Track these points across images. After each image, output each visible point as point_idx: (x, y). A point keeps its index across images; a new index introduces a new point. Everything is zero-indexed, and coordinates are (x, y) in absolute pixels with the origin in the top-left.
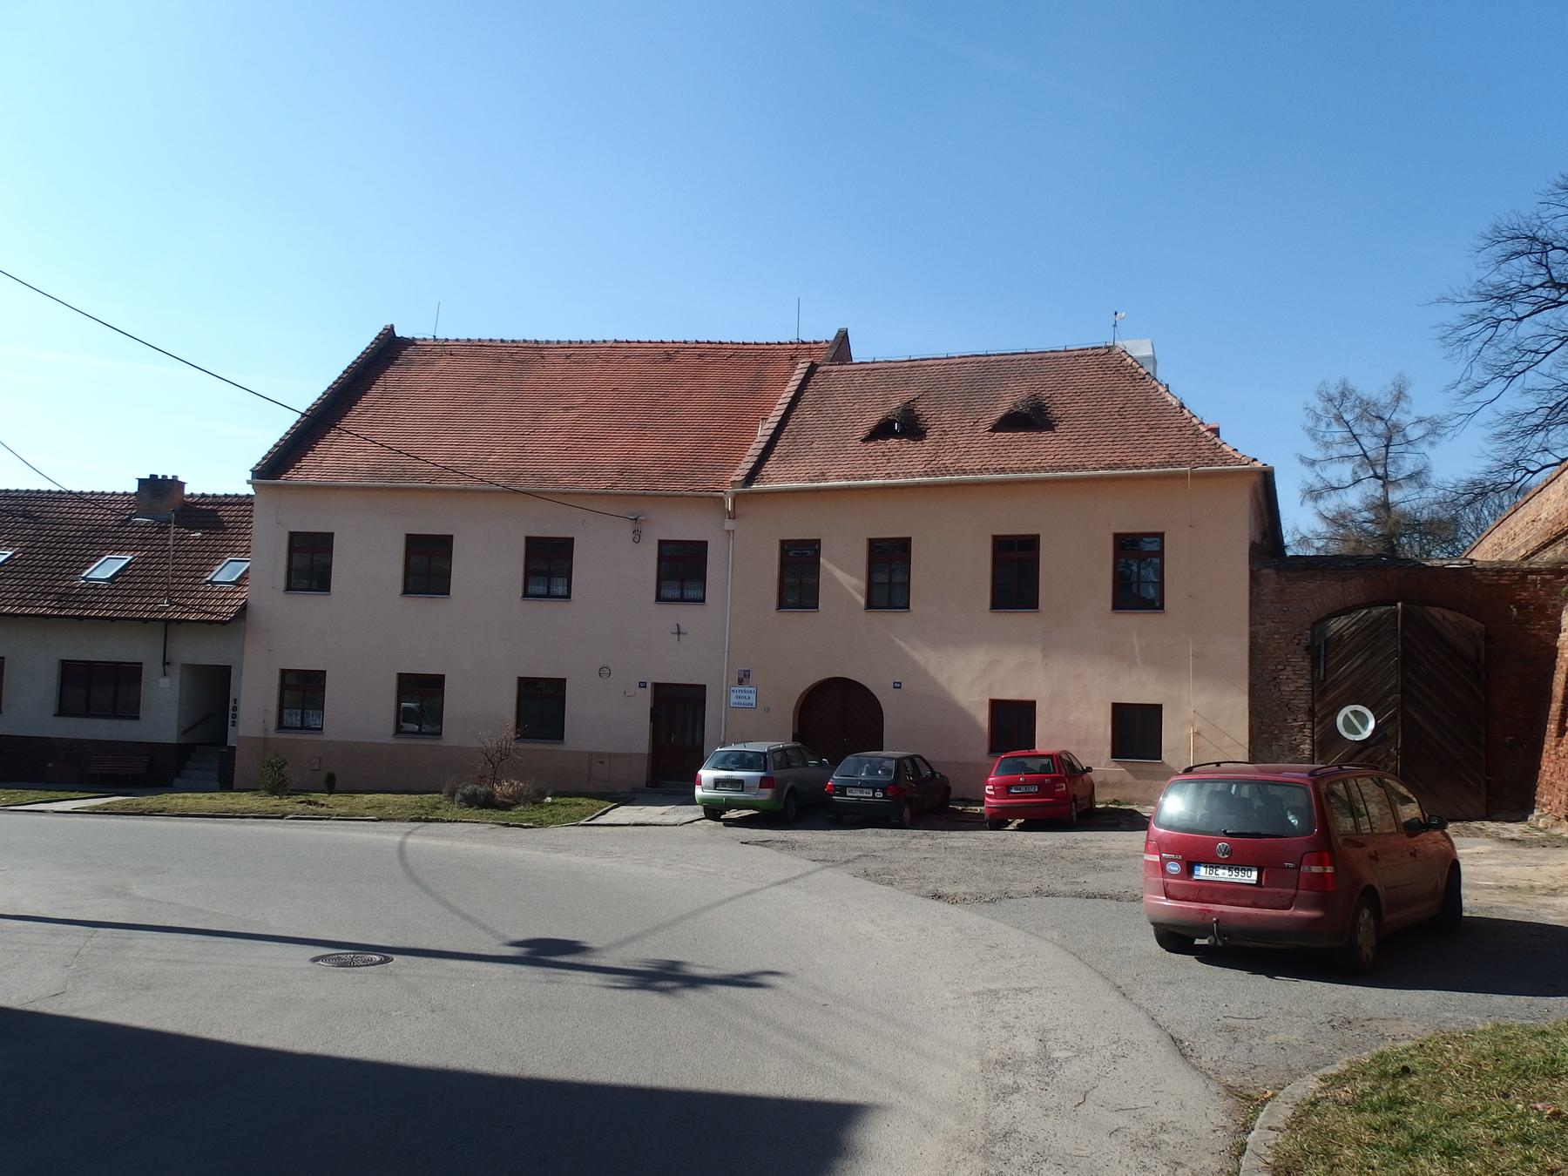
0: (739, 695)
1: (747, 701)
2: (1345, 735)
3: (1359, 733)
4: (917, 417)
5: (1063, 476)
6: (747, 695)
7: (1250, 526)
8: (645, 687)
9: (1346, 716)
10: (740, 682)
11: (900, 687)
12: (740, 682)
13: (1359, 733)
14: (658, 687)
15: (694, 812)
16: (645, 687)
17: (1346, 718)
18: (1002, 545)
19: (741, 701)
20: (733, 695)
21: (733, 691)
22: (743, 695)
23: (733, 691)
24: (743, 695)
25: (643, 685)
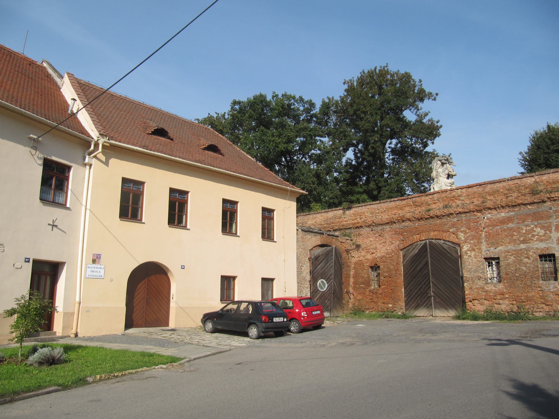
0: (93, 270)
1: (98, 274)
2: (325, 282)
3: (323, 289)
4: (529, 150)
5: (225, 172)
6: (99, 270)
7: (500, 179)
8: (29, 262)
9: (325, 288)
10: (94, 261)
11: (184, 268)
12: (94, 261)
13: (323, 289)
14: (36, 263)
15: (437, 97)
16: (29, 262)
17: (325, 287)
18: (264, 210)
19: (94, 274)
20: (89, 270)
21: (89, 267)
22: (96, 270)
23: (89, 267)
24: (96, 270)
25: (27, 260)
